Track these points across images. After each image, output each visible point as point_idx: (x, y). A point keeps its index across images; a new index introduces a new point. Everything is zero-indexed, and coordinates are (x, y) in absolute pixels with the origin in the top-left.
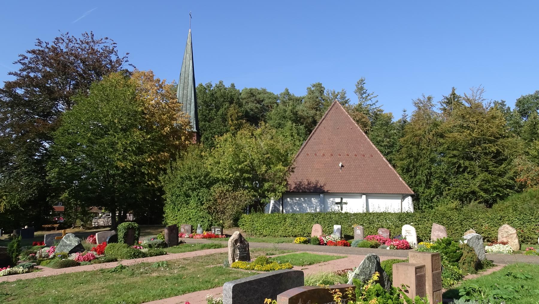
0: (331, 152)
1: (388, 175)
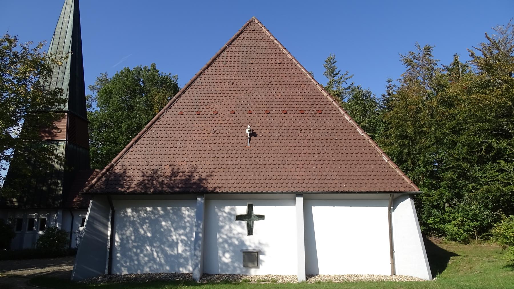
0: (233, 106)
1: (356, 151)
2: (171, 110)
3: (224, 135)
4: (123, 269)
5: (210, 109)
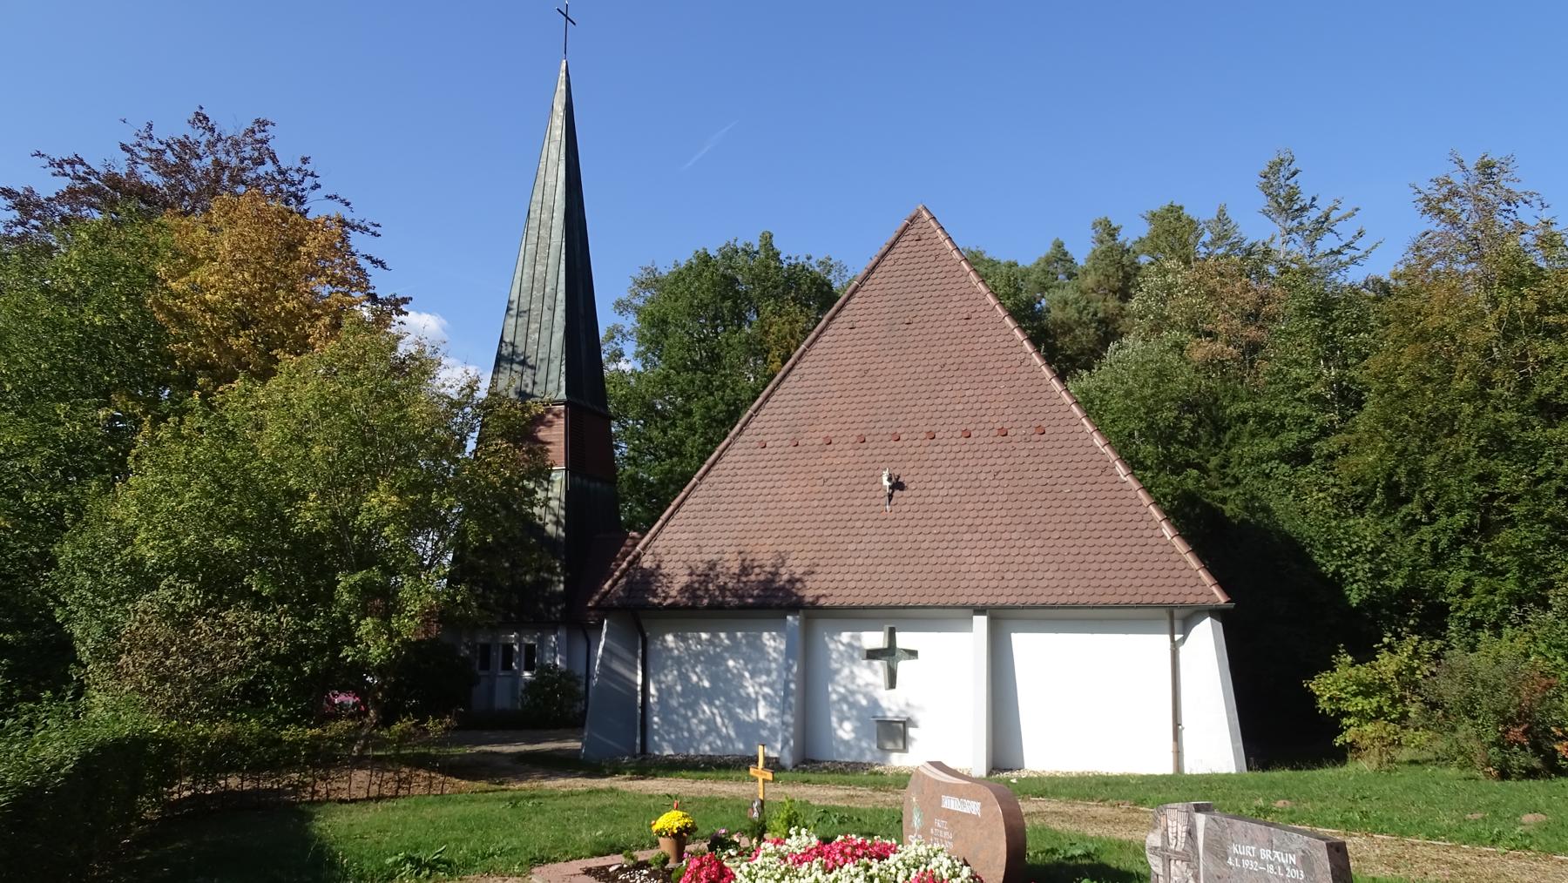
2: (742, 438)
3: (842, 488)
4: (665, 744)
5: (817, 434)
